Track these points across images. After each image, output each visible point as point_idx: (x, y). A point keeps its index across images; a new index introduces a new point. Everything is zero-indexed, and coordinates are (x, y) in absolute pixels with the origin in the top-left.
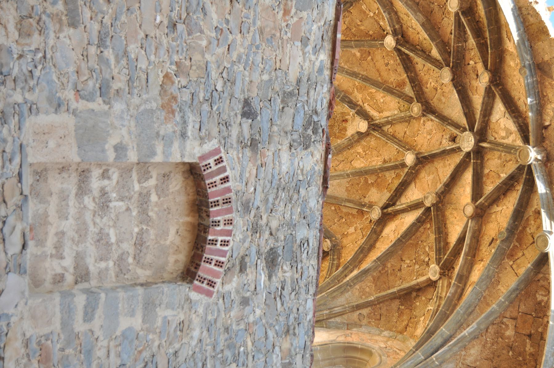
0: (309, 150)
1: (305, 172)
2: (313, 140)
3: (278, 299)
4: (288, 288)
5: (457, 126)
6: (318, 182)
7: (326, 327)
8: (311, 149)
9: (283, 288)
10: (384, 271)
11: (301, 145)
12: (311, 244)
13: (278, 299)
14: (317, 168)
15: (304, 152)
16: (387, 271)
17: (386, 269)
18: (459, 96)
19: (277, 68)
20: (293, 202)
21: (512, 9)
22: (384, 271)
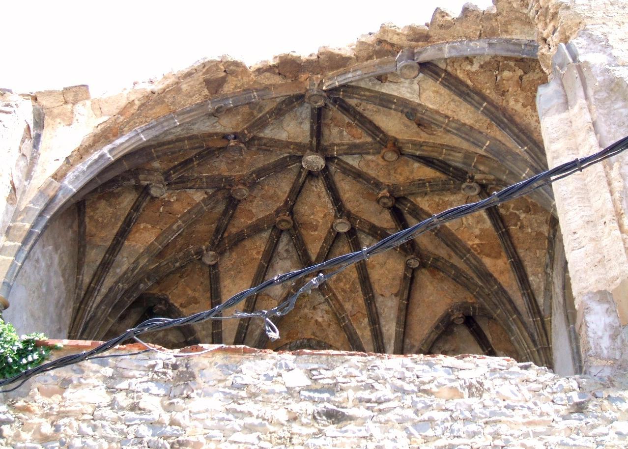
0: (196, 373)
1: (223, 377)
2: (185, 369)
3: (382, 407)
4: (366, 395)
5: (340, 155)
6: (238, 360)
7: (551, 316)
8: (196, 371)
9: (369, 401)
10: (478, 248)
11: (187, 384)
12: (316, 366)
13: (382, 407)
14: (220, 362)
15: (199, 380)
16: (478, 245)
17: (475, 246)
18: (491, 222)
19: (92, 417)
20: (258, 392)
21: (217, 77)
22: (478, 248)
